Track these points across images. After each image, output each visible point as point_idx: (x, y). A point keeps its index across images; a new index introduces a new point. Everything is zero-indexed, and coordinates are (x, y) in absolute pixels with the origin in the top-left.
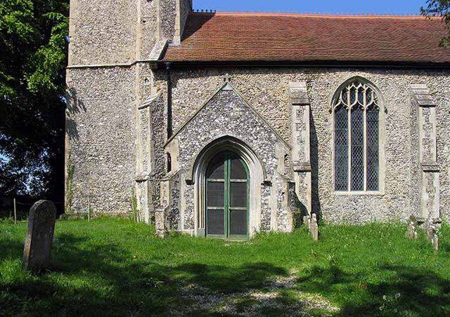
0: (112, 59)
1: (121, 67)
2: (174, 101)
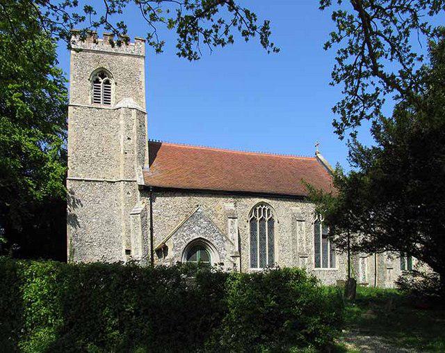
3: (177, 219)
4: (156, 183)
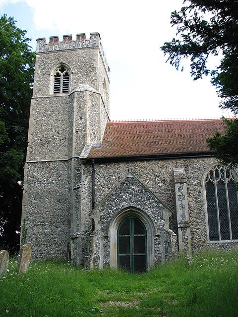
1: (60, 161)
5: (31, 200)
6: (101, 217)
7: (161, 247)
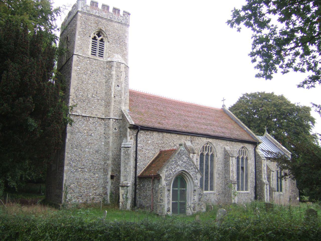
0: (94, 113)
1: (99, 118)
2: (139, 145)
3: (153, 152)
4: (141, 124)
5: (72, 148)
6: (166, 176)
7: (196, 198)
